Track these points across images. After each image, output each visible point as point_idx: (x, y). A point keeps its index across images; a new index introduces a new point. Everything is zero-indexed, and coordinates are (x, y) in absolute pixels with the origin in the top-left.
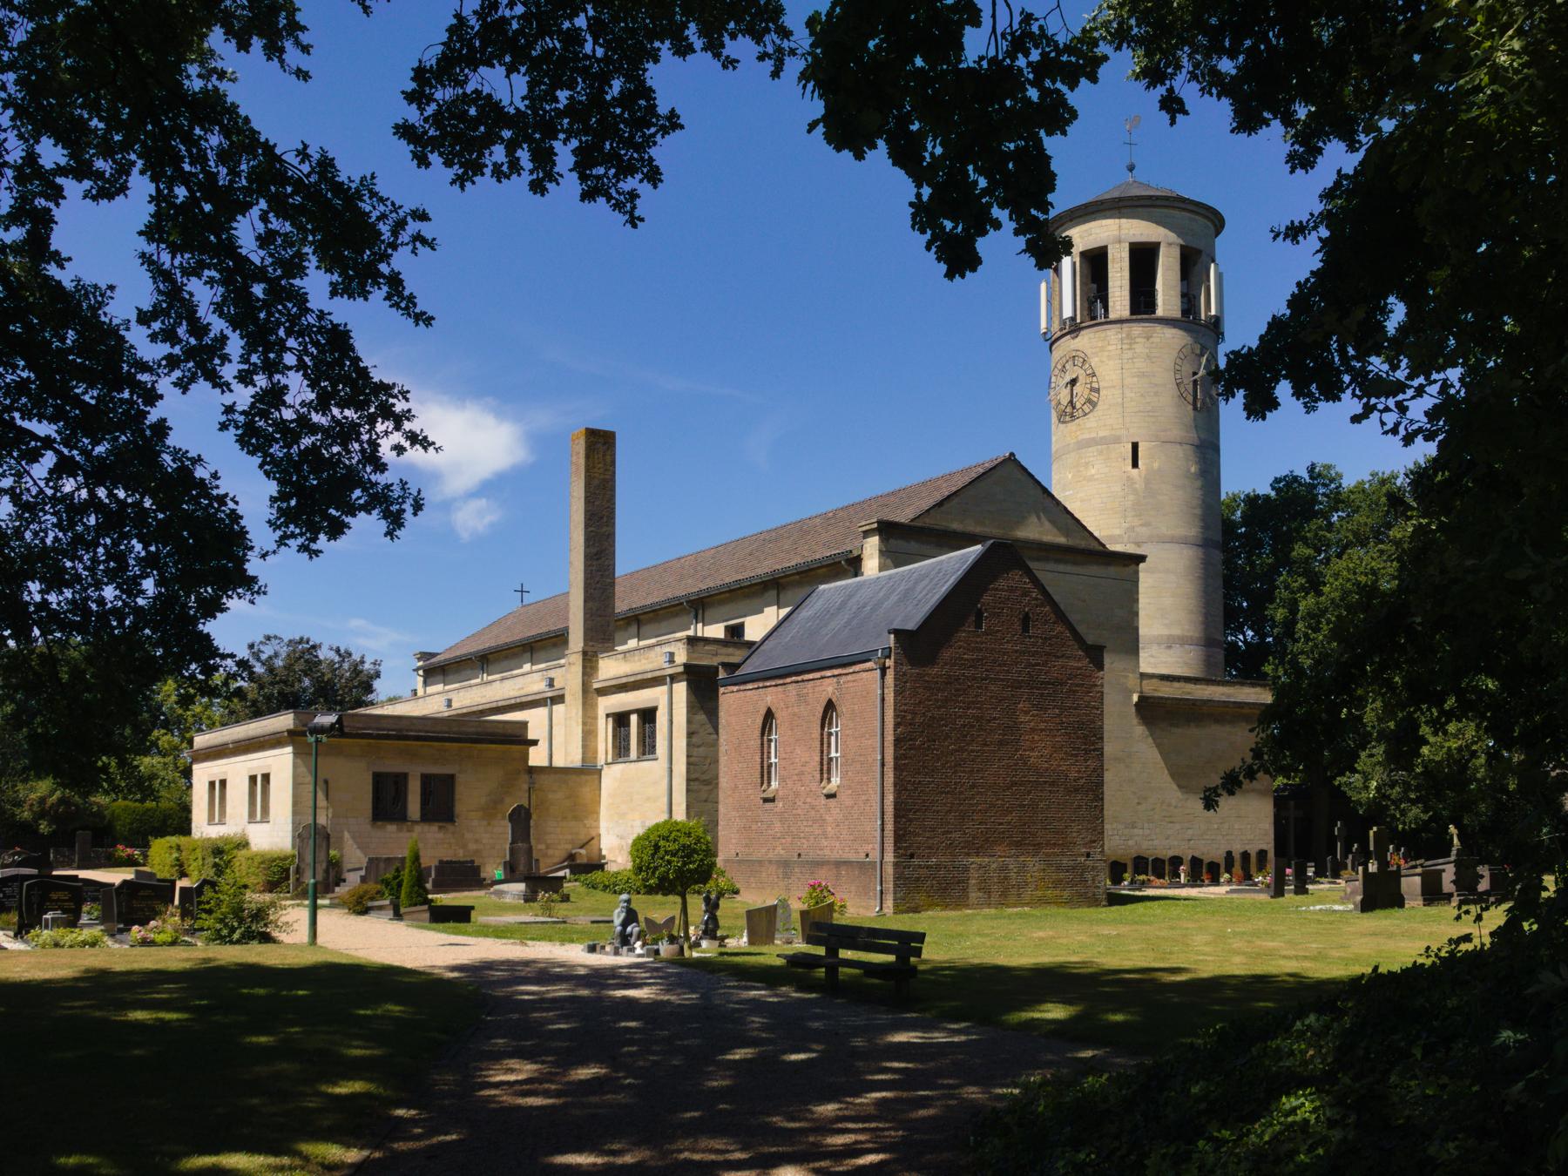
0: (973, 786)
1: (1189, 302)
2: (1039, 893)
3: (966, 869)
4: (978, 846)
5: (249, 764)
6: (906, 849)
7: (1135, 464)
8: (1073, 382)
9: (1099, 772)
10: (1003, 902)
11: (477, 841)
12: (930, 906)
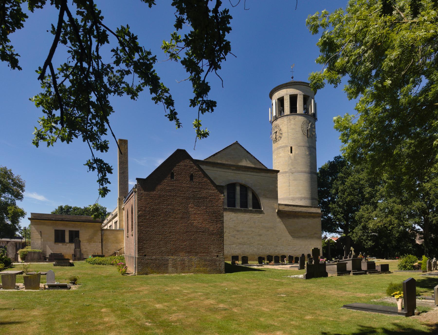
0: (170, 232)
1: (306, 109)
2: (197, 269)
3: (167, 260)
4: (174, 252)
6: (143, 253)
7: (291, 152)
8: (276, 132)
9: (222, 228)
10: (183, 270)
11: (86, 248)
12: (152, 273)
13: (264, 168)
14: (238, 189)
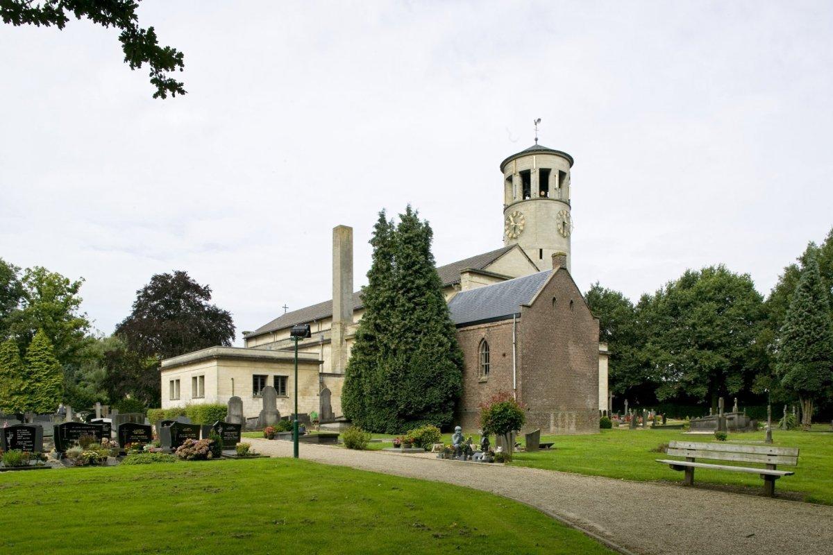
5: (192, 372)
7: (541, 258)
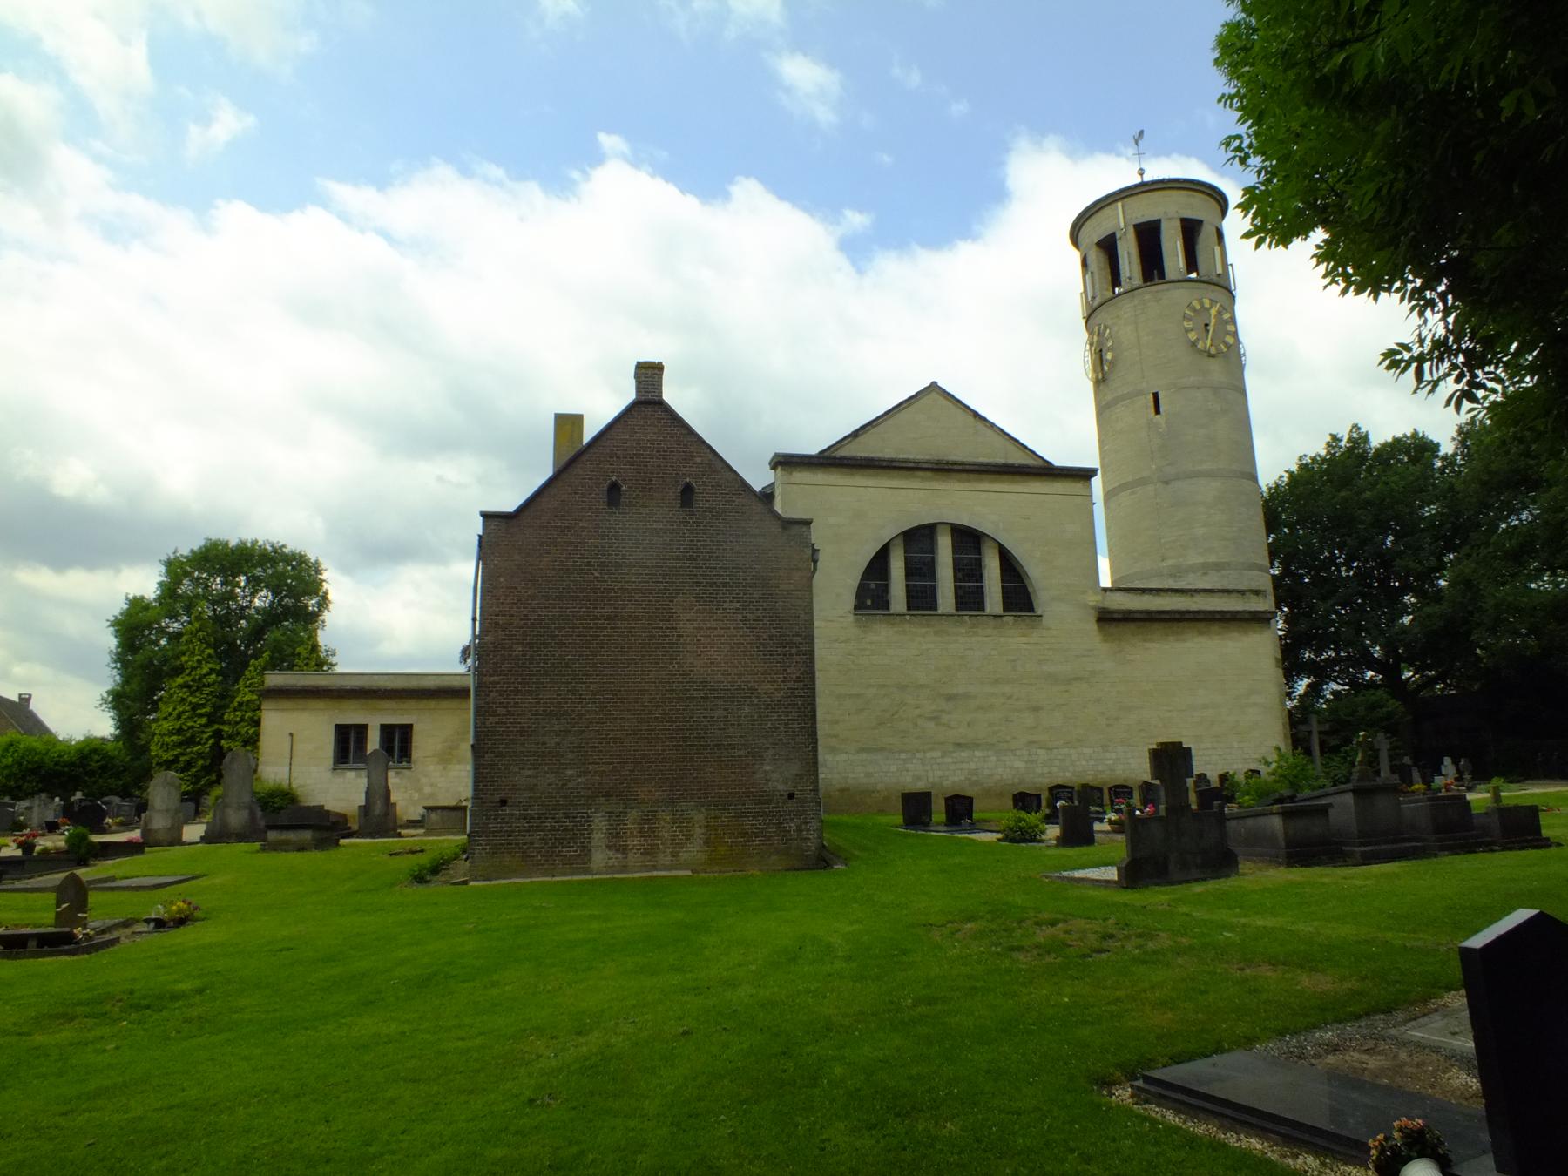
7: (1158, 411)
13: (1040, 463)
14: (944, 544)
